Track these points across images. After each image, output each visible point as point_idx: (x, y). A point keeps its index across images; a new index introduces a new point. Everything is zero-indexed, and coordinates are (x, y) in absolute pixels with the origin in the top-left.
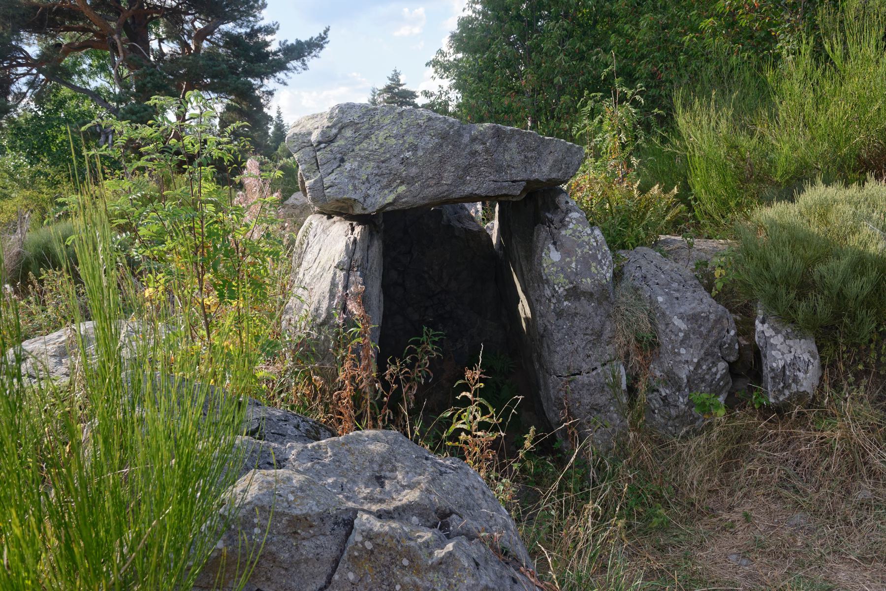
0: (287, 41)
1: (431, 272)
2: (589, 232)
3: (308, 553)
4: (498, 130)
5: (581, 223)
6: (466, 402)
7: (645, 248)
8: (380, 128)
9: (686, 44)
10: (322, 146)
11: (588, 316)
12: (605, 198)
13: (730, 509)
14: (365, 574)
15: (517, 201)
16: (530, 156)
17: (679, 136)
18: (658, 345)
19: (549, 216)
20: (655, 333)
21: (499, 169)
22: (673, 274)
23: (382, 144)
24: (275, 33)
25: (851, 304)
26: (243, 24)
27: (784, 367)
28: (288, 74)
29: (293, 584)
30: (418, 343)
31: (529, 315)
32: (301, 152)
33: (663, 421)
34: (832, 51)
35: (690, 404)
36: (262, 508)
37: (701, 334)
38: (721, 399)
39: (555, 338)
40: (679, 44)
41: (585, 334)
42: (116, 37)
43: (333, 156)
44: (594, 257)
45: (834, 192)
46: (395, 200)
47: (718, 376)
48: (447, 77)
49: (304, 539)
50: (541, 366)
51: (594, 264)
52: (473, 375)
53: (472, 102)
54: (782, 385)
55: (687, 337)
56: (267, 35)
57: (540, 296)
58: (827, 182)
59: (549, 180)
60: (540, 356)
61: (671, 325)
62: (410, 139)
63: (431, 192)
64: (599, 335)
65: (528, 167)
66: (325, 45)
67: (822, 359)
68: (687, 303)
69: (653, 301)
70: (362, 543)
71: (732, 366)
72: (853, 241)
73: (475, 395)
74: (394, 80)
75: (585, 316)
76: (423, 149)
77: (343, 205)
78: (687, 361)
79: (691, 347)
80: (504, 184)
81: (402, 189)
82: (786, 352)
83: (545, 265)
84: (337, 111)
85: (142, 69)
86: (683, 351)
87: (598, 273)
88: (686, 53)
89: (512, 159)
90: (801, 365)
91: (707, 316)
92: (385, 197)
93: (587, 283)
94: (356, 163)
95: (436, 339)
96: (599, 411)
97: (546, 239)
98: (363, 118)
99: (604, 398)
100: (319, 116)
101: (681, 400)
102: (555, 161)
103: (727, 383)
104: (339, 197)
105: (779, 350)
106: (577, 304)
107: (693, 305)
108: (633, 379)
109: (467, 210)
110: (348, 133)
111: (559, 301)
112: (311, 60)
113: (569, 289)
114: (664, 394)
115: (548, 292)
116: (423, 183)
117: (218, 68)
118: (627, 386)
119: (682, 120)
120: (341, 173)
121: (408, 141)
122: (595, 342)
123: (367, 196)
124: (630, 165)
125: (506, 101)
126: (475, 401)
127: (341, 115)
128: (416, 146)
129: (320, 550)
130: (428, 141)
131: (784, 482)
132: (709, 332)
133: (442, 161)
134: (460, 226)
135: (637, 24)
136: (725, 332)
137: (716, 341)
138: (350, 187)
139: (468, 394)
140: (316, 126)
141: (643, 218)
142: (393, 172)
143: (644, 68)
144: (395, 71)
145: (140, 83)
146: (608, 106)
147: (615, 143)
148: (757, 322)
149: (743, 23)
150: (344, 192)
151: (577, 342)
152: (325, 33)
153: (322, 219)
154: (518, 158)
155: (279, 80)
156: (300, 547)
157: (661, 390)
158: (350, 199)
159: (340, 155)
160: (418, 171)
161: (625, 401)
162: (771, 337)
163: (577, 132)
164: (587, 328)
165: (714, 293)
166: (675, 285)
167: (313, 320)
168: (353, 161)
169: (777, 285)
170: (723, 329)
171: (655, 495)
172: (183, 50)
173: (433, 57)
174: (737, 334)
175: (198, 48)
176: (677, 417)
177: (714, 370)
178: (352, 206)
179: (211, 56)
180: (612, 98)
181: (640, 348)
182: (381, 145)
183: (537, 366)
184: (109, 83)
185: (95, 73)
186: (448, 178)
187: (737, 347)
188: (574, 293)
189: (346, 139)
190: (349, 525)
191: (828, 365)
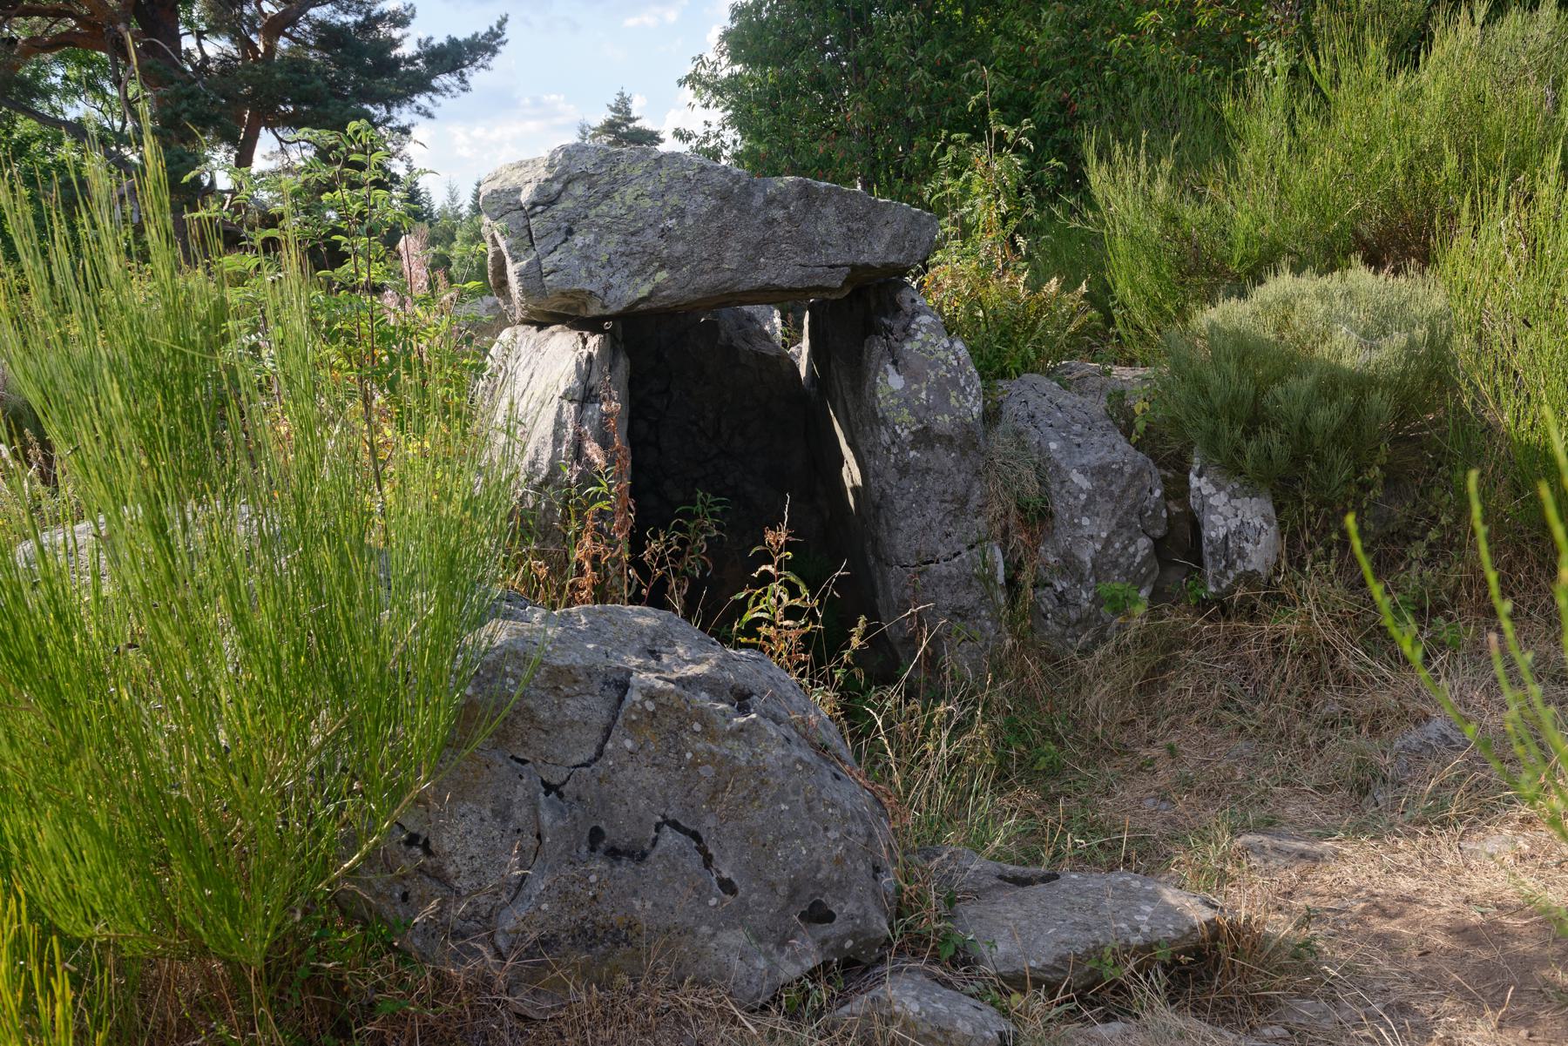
0: (431, 38)
1: (701, 423)
2: (947, 345)
3: (573, 713)
4: (807, 187)
5: (934, 331)
6: (767, 578)
7: (1035, 376)
8: (628, 182)
9: (1115, 52)
10: (539, 209)
11: (946, 473)
12: (975, 302)
13: (1150, 742)
14: (646, 741)
15: (836, 300)
16: (855, 227)
17: (1093, 206)
18: (1051, 515)
19: (887, 322)
20: (1045, 495)
21: (809, 247)
22: (1075, 412)
23: (631, 207)
24: (408, 23)
25: (1317, 442)
26: (349, 6)
27: (1226, 537)
28: (434, 97)
29: (556, 751)
30: (690, 516)
31: (859, 482)
32: (505, 218)
33: (1058, 629)
34: (1319, 71)
35: (1098, 600)
36: (516, 654)
37: (1111, 495)
38: (1144, 594)
39: (898, 506)
40: (1105, 53)
41: (942, 501)
42: (121, 27)
43: (555, 226)
44: (954, 383)
45: (1309, 283)
46: (652, 293)
47: (1138, 559)
48: (716, 106)
49: (567, 696)
50: (879, 559)
51: (954, 394)
52: (777, 537)
53: (762, 148)
54: (1224, 563)
55: (1091, 500)
56: (395, 26)
57: (874, 445)
58: (1297, 270)
59: (885, 265)
60: (876, 541)
61: (1069, 483)
62: (673, 199)
63: (706, 281)
64: (963, 501)
65: (854, 245)
66: (501, 48)
67: (1282, 524)
68: (1092, 452)
69: (1042, 449)
70: (642, 703)
71: (1158, 544)
72: (1323, 351)
73: (779, 568)
74: (619, 111)
75: (942, 473)
76: (694, 215)
77: (571, 301)
78: (1092, 537)
79: (1098, 515)
80: (819, 270)
81: (662, 276)
82: (1231, 515)
83: (880, 396)
84: (561, 155)
85: (173, 88)
86: (1085, 521)
87: (961, 406)
88: (1114, 68)
89: (829, 233)
90: (1250, 533)
91: (1121, 469)
92: (636, 289)
93: (943, 421)
94: (592, 237)
95: (718, 509)
96: (964, 618)
97: (882, 356)
98: (601, 167)
99: (971, 597)
100: (530, 165)
101: (1084, 595)
102: (894, 236)
103: (1151, 572)
104: (567, 287)
105: (1221, 514)
106: (930, 455)
107: (1100, 454)
108: (1014, 568)
109: (758, 323)
110: (579, 189)
111: (902, 450)
112: (475, 73)
113: (917, 431)
114: (1059, 589)
115: (885, 438)
116: (694, 267)
117: (309, 87)
118: (1007, 580)
119: (1097, 176)
120: (569, 251)
121: (672, 202)
122: (958, 513)
123: (608, 287)
124: (1016, 249)
125: (820, 148)
126: (781, 576)
127: (566, 162)
128: (683, 210)
129: (587, 713)
130: (702, 204)
131: (1227, 703)
132: (1124, 492)
133: (723, 233)
134: (747, 347)
135: (1037, 19)
136: (1146, 493)
137: (1133, 506)
138: (583, 273)
139: (770, 568)
140: (527, 179)
141: (1032, 330)
142: (648, 250)
143: (1047, 95)
144: (622, 94)
145: (169, 111)
146: (980, 155)
147: (989, 214)
148: (1192, 475)
149: (1203, 21)
150: (574, 280)
151: (930, 513)
152: (500, 25)
153: (528, 333)
154: (838, 231)
155: (419, 108)
156: (563, 706)
157: (1056, 583)
158: (582, 292)
159: (566, 224)
160: (686, 248)
161: (1002, 601)
162: (1210, 495)
163: (932, 195)
164: (945, 492)
165: (1134, 438)
166: (1077, 428)
167: (529, 479)
168: (588, 232)
169: (1218, 418)
170: (1144, 488)
171: (1044, 731)
172: (244, 53)
173: (690, 69)
174: (1166, 496)
175: (270, 49)
176: (1079, 621)
177: (1132, 550)
178: (584, 304)
179: (296, 65)
180: (986, 143)
181: (1024, 522)
182: (630, 208)
183: (872, 561)
184: (100, 110)
185: (76, 93)
186: (732, 259)
187: (1164, 515)
188: (925, 438)
189: (576, 199)
190: (623, 686)
191: (1291, 537)
